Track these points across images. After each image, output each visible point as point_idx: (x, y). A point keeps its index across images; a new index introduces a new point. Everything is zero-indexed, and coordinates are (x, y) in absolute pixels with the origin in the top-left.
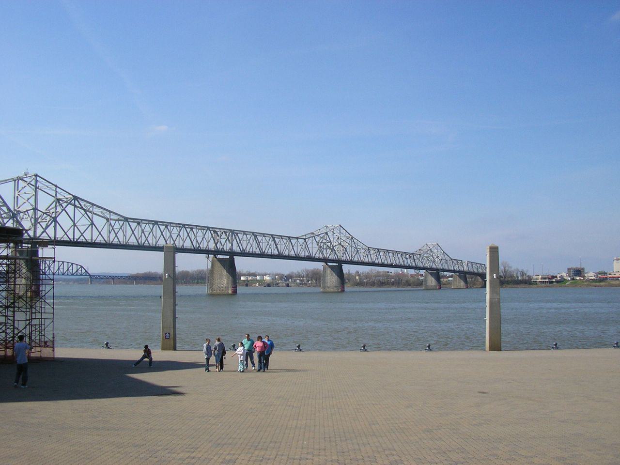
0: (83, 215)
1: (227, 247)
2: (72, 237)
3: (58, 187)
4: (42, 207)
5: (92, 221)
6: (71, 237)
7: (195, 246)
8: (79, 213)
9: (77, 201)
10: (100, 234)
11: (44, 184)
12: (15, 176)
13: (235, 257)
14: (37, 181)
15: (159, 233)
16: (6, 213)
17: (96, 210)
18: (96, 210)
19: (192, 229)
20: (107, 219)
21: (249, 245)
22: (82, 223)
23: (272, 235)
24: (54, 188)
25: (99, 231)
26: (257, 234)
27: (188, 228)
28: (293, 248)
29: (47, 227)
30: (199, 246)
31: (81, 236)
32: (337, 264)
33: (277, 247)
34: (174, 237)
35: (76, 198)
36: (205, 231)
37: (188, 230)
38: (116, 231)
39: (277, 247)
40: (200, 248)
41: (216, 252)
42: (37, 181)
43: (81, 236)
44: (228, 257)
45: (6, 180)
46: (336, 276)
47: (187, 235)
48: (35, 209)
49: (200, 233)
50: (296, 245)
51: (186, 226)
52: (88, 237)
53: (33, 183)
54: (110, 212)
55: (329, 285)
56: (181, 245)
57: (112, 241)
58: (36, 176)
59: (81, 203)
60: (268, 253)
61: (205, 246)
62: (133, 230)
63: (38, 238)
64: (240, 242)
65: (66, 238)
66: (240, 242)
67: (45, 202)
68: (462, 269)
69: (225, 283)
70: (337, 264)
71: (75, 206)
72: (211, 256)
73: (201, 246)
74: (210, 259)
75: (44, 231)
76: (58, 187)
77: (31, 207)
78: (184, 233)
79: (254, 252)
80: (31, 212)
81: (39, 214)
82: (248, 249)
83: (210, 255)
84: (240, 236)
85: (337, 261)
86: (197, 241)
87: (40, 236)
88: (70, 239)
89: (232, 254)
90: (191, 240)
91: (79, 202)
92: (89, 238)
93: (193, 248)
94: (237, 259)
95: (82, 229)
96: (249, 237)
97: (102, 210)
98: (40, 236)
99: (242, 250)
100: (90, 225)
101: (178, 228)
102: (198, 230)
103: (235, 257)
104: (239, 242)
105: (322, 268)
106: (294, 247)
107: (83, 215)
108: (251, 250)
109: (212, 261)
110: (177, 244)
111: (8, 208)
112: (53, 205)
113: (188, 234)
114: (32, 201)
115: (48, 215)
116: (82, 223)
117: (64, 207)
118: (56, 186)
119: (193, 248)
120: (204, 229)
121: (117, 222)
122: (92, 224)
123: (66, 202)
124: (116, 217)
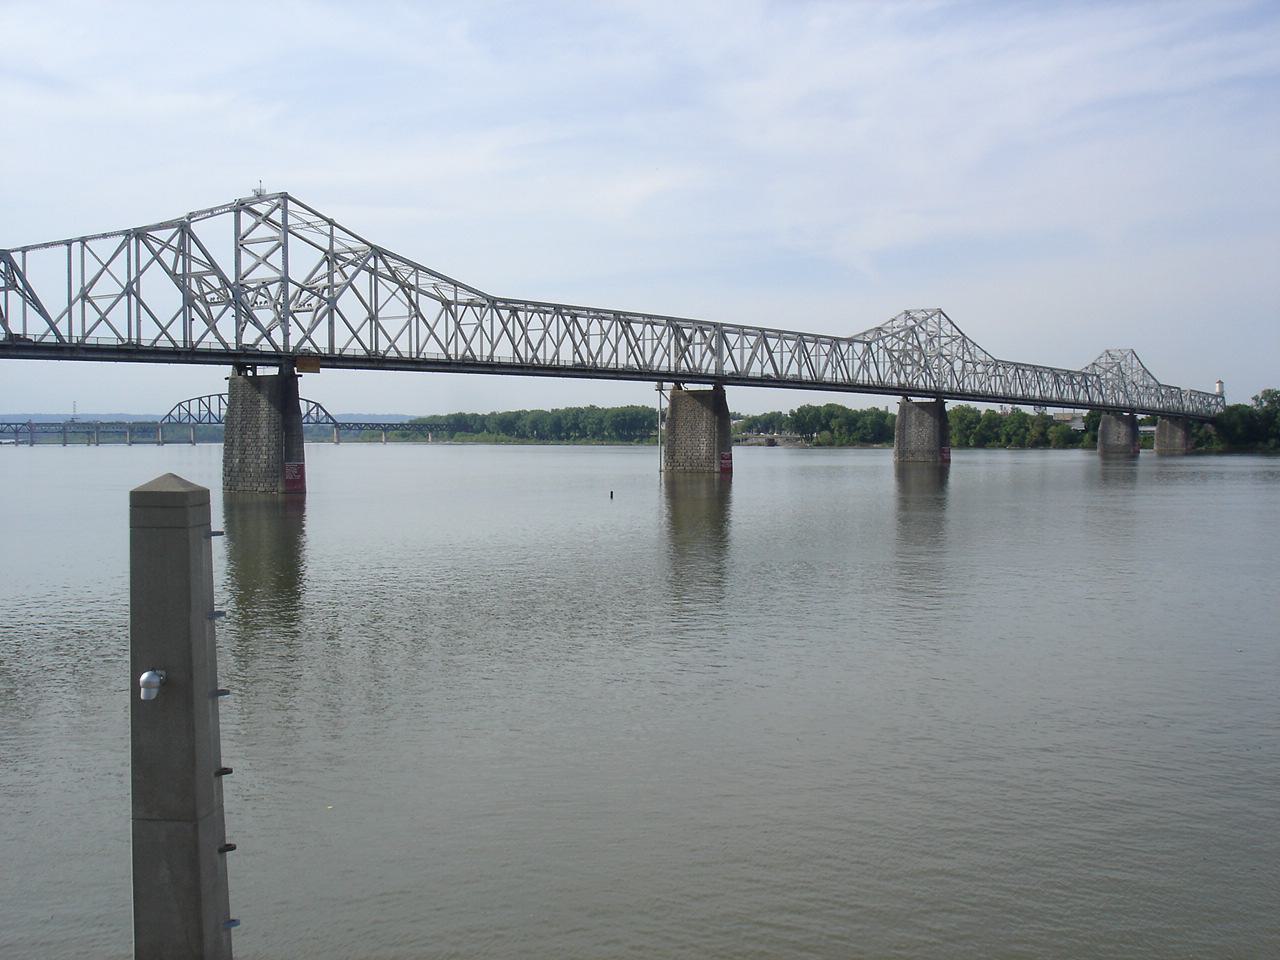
0: (394, 294)
1: (709, 365)
2: (454, 353)
3: (337, 226)
4: (298, 274)
5: (417, 308)
6: (280, 342)
7: (523, 356)
8: (386, 288)
9: (382, 258)
10: (355, 335)
11: (301, 219)
12: (230, 199)
13: (726, 387)
14: (285, 213)
15: (498, 326)
16: (216, 291)
17: (426, 282)
18: (426, 282)
19: (574, 317)
20: (447, 304)
21: (660, 351)
22: (394, 308)
23: (670, 321)
24: (327, 229)
25: (435, 336)
26: (516, 305)
27: (502, 308)
28: (731, 354)
29: (315, 323)
30: (535, 356)
31: (160, 335)
32: (933, 400)
33: (771, 358)
34: (468, 331)
35: (378, 252)
36: (548, 316)
37: (505, 314)
38: (468, 333)
39: (771, 358)
40: (538, 360)
41: (677, 377)
42: (285, 213)
43: (160, 335)
44: (710, 387)
45: (211, 210)
46: (931, 418)
47: (565, 327)
48: (285, 280)
49: (536, 322)
50: (738, 345)
51: (499, 304)
52: (404, 348)
53: (277, 216)
54: (456, 284)
55: (913, 446)
56: (487, 352)
57: (659, 366)
58: (285, 197)
59: (391, 265)
60: (661, 369)
61: (549, 357)
62: (431, 326)
63: (193, 348)
64: (637, 344)
65: (164, 343)
66: (637, 344)
67: (304, 262)
68: (1098, 399)
69: (704, 448)
70: (933, 400)
71: (373, 271)
72: (669, 386)
73: (540, 355)
74: (668, 394)
75: (307, 337)
76: (337, 226)
77: (277, 275)
78: (493, 322)
79: (673, 370)
80: (274, 289)
81: (292, 289)
82: (605, 359)
83: (664, 383)
84: (637, 328)
85: (934, 392)
86: (528, 341)
87: (199, 342)
88: (173, 342)
89: (720, 380)
90: (513, 344)
91: (385, 262)
92: (322, 344)
93: (518, 361)
94: (731, 391)
95: (103, 305)
96: (658, 329)
97: (436, 280)
98: (199, 342)
99: (641, 363)
100: (121, 296)
101: (477, 309)
102: (529, 314)
103: (726, 387)
104: (633, 343)
105: (894, 410)
106: (733, 351)
107: (394, 294)
108: (665, 363)
109: (671, 396)
110: (477, 353)
111: (223, 279)
112: (324, 269)
113: (505, 325)
114: (276, 259)
115: (315, 294)
116: (394, 308)
117: (349, 275)
118: (331, 223)
119: (518, 361)
120: (547, 312)
121: (469, 308)
122: (418, 315)
123: (353, 263)
124: (463, 296)
